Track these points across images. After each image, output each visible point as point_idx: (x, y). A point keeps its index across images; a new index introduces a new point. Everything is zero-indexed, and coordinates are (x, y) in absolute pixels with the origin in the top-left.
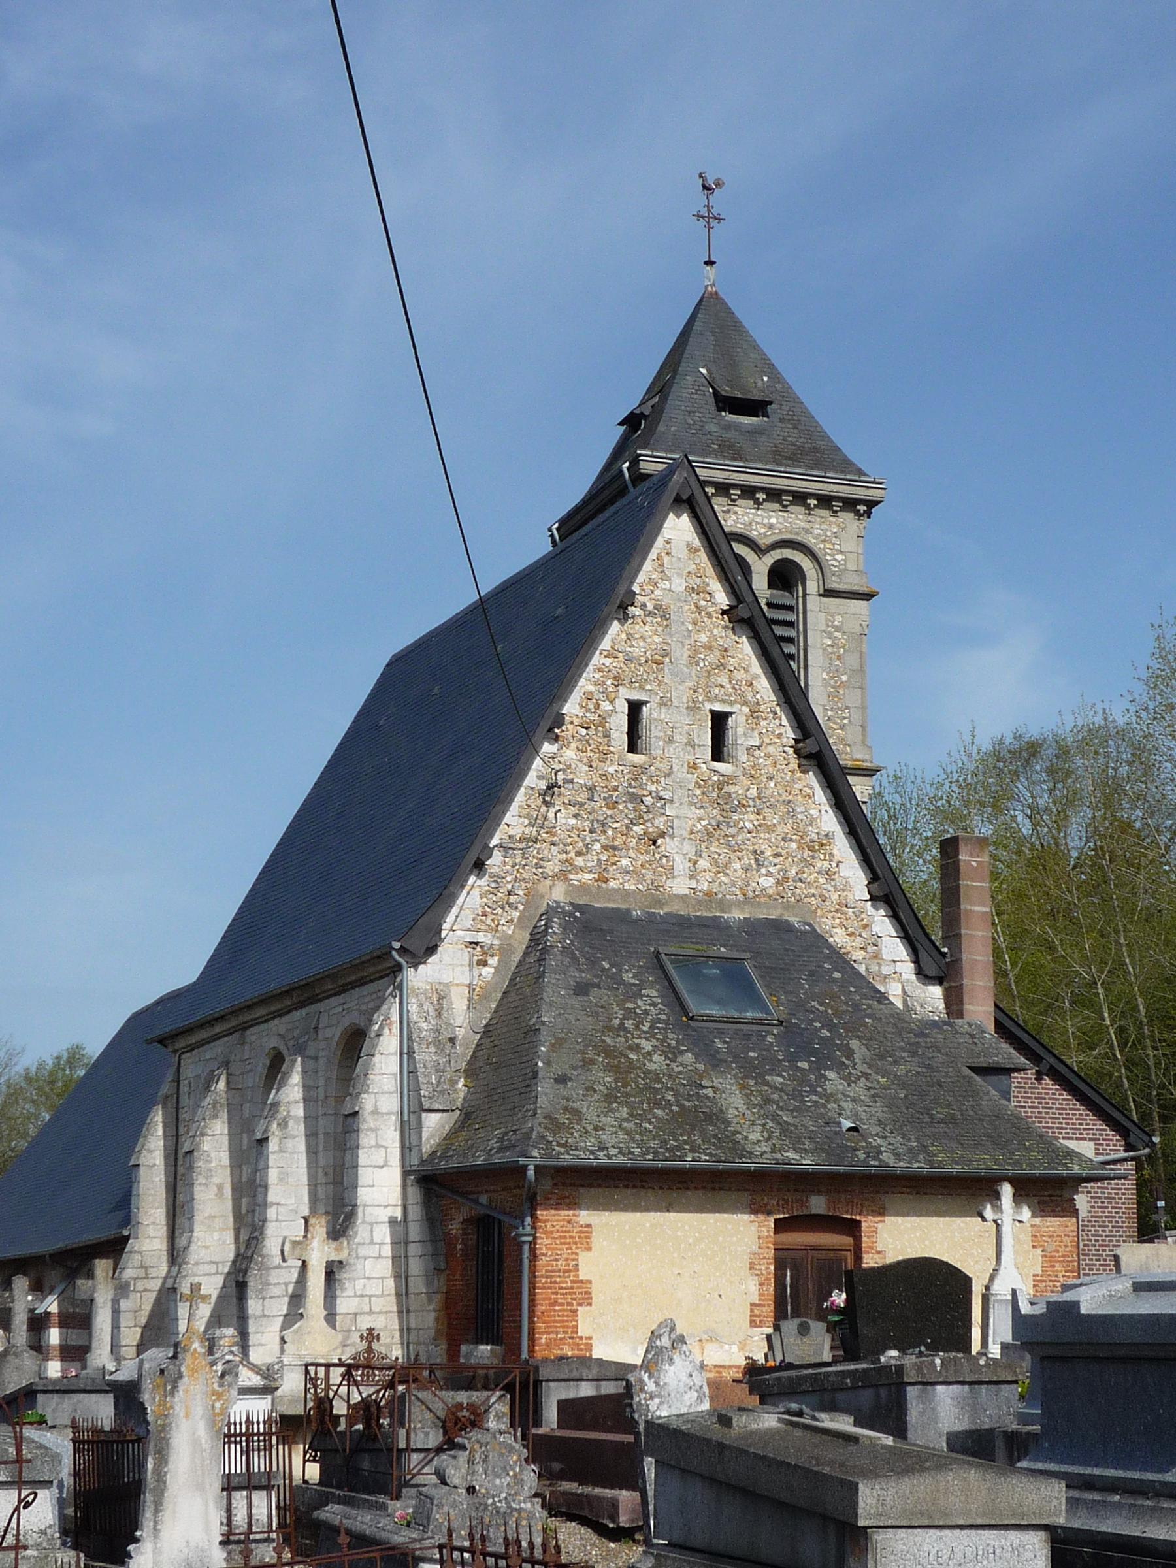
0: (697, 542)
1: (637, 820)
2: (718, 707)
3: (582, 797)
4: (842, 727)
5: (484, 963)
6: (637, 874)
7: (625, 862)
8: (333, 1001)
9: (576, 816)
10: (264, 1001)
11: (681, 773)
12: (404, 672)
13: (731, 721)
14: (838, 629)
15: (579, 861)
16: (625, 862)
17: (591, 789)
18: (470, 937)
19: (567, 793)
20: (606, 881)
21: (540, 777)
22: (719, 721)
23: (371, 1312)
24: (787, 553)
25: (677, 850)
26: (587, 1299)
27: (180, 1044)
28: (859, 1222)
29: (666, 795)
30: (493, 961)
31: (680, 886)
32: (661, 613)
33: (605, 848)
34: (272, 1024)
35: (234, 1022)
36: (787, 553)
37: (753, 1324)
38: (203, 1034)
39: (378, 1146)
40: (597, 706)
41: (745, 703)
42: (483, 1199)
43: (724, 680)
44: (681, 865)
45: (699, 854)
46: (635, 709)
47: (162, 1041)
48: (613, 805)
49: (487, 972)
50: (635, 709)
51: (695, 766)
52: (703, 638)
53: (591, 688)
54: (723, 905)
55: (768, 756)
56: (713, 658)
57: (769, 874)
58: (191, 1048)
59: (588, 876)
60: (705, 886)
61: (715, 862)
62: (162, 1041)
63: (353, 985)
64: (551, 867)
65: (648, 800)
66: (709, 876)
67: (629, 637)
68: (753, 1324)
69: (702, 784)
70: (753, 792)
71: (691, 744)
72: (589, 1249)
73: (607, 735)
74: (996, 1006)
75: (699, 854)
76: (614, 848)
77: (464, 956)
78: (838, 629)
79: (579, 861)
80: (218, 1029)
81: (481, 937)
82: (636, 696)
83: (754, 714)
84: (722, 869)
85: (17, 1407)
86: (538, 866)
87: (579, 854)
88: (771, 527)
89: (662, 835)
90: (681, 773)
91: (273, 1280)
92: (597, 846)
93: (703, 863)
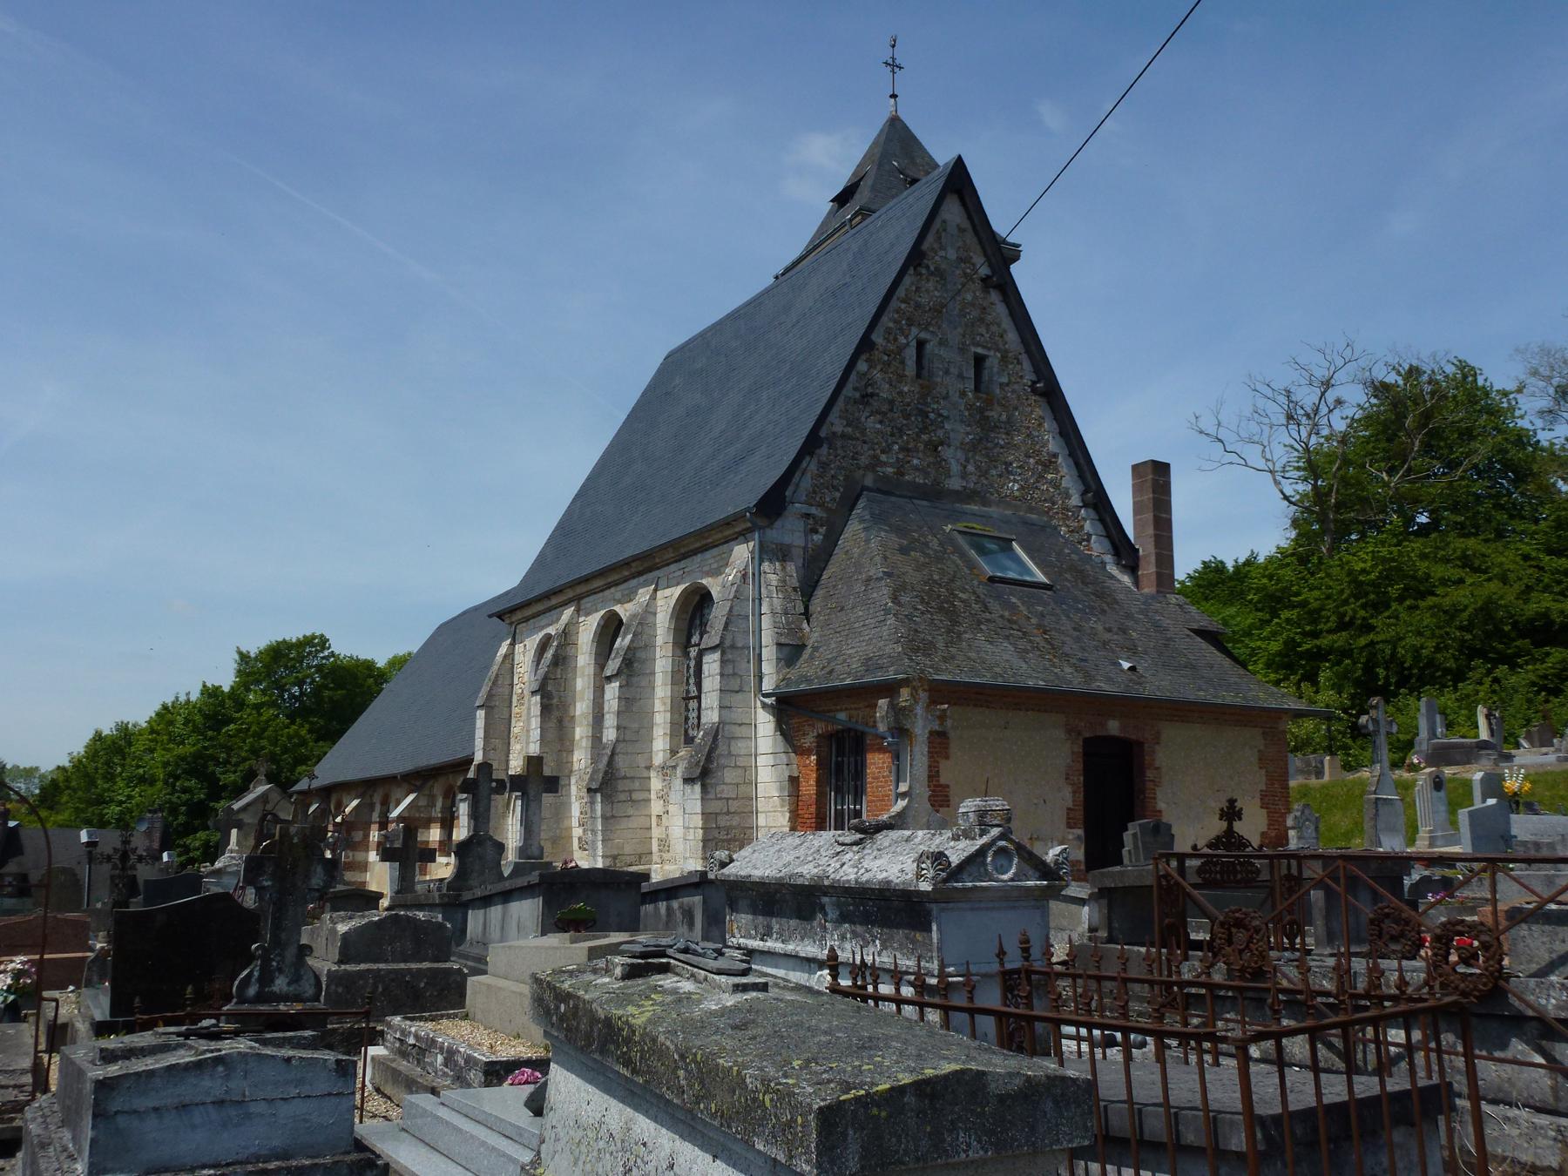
0: (966, 224)
1: (924, 430)
2: (980, 350)
3: (885, 408)
5: (816, 532)
7: (915, 461)
8: (673, 567)
9: (881, 422)
10: (601, 573)
11: (955, 397)
12: (675, 363)
13: (988, 363)
15: (883, 458)
16: (915, 461)
17: (891, 402)
18: (804, 509)
19: (875, 404)
20: (903, 475)
21: (855, 389)
22: (979, 361)
23: (728, 813)
25: (952, 456)
27: (519, 616)
29: (945, 413)
30: (822, 530)
32: (939, 274)
33: (902, 449)
34: (607, 593)
35: (570, 594)
37: (1069, 826)
38: (540, 607)
39: (735, 674)
40: (896, 339)
41: (998, 350)
42: (842, 716)
44: (955, 468)
45: (967, 460)
46: (921, 345)
47: (500, 616)
48: (907, 416)
49: (817, 538)
50: (921, 345)
53: (891, 325)
55: (1013, 391)
56: (975, 313)
57: (1015, 481)
58: (527, 619)
59: (890, 470)
61: (978, 468)
62: (500, 616)
63: (695, 552)
64: (864, 460)
65: (932, 416)
66: (974, 478)
67: (918, 289)
68: (1069, 826)
69: (970, 407)
70: (1004, 417)
71: (961, 376)
72: (947, 758)
73: (903, 362)
75: (967, 460)
76: (908, 450)
77: (800, 525)
79: (883, 458)
80: (554, 601)
81: (813, 510)
82: (923, 335)
83: (1004, 359)
86: (853, 458)
87: (883, 452)
89: (942, 444)
90: (955, 397)
91: (620, 788)
92: (896, 447)
93: (970, 468)
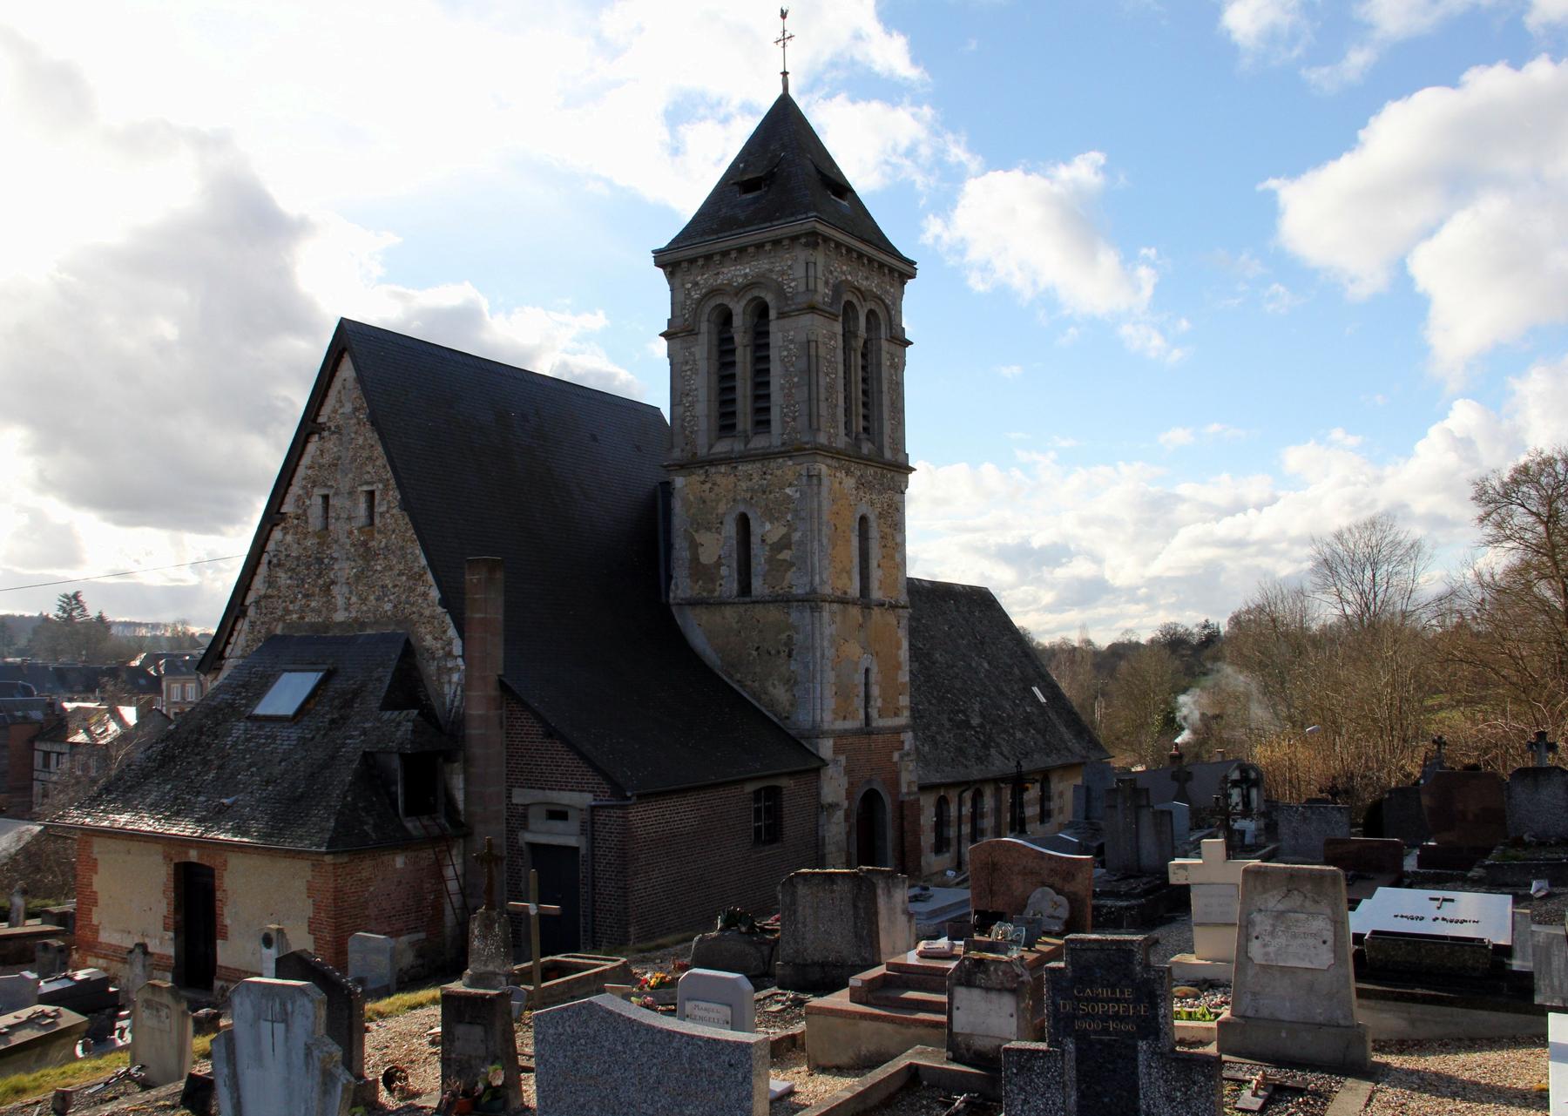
1: (319, 576)
2: (366, 488)
4: (794, 419)
6: (319, 612)
14: (792, 341)
24: (756, 293)
26: (95, 903)
28: (1420, 866)
31: (340, 616)
36: (756, 293)
37: (166, 929)
43: (369, 468)
44: (340, 601)
51: (351, 532)
52: (360, 441)
54: (363, 625)
60: (354, 614)
74: (503, 686)
78: (792, 341)
84: (364, 600)
85: (15, 953)
88: (746, 275)
93: (354, 599)
